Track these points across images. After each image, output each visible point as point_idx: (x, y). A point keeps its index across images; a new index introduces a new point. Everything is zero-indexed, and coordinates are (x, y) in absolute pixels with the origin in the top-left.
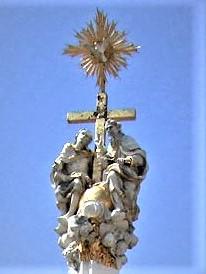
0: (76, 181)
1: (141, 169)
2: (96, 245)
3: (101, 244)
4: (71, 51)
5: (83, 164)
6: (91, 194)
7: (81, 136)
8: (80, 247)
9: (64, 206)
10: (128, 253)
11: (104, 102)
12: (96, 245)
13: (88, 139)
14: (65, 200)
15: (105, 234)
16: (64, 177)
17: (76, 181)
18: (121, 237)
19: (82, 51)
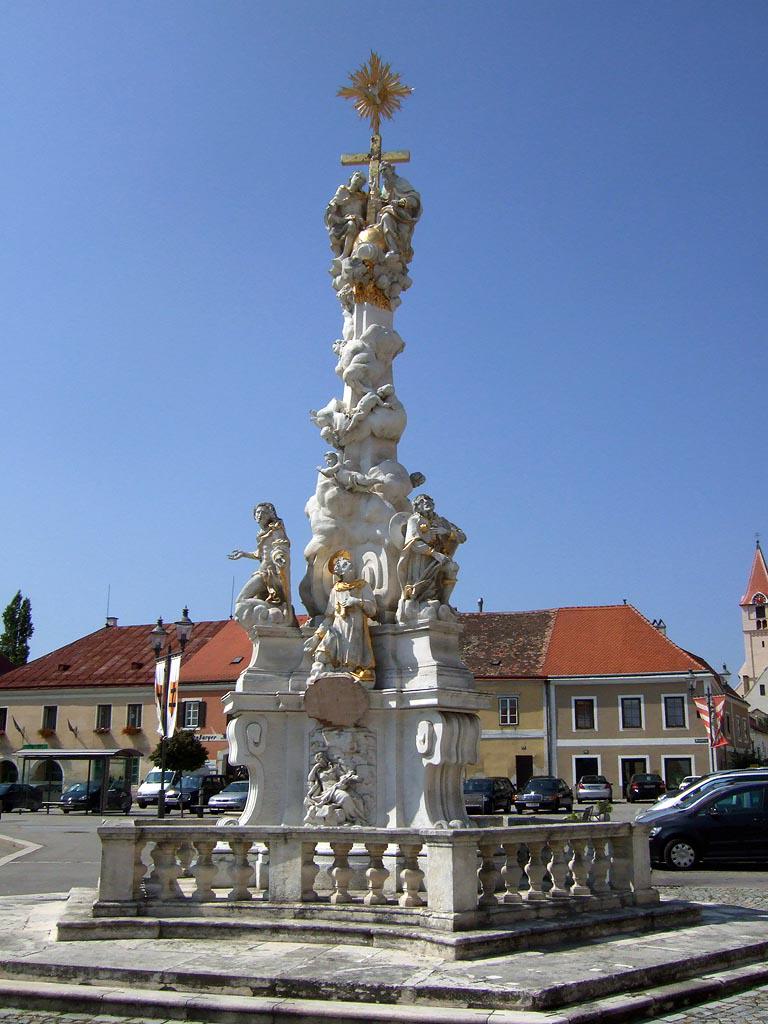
1: (415, 211)
3: (375, 286)
5: (357, 206)
12: (370, 287)
13: (362, 181)
14: (339, 242)
15: (379, 276)
17: (350, 223)
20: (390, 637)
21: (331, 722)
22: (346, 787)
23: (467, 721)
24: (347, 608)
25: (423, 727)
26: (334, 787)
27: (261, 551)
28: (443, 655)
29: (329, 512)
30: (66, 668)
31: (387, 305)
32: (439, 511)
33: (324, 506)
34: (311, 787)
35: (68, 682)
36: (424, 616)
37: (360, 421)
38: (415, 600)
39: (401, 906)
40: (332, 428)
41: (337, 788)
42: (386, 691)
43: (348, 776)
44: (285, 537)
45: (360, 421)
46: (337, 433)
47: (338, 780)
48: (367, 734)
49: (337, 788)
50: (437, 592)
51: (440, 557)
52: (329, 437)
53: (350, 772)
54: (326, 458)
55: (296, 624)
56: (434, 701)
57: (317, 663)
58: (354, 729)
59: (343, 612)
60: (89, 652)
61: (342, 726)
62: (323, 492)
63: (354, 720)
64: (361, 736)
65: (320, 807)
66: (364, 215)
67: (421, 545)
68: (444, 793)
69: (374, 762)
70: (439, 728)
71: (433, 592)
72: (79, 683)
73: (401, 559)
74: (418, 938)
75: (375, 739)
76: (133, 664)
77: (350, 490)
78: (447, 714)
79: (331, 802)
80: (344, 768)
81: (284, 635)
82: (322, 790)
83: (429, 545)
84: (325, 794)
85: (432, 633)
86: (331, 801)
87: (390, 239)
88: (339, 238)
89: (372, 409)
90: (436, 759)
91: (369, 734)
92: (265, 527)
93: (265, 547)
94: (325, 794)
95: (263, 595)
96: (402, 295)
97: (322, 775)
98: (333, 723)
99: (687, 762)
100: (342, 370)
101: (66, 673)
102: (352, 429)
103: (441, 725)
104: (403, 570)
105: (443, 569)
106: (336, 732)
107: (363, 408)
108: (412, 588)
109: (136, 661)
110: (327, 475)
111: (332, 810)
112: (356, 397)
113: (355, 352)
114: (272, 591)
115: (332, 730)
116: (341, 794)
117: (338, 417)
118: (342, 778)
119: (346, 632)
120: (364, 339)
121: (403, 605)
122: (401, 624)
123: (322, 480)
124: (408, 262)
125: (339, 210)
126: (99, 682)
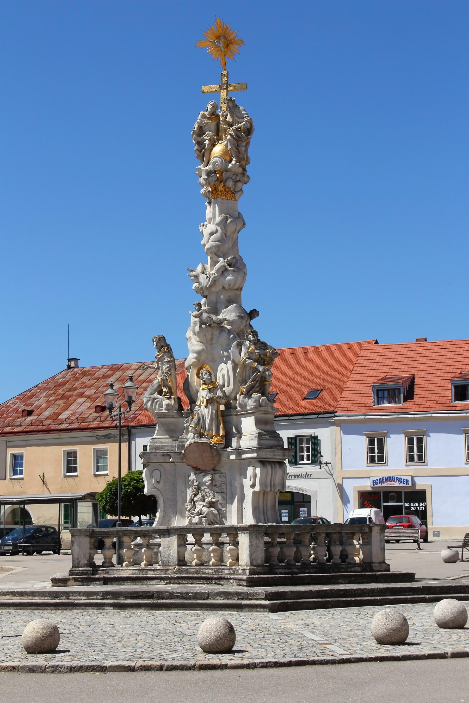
0: (207, 142)
1: (249, 131)
2: (221, 188)
3: (224, 186)
4: (241, 565)
5: (213, 125)
6: (218, 149)
7: (209, 107)
8: (210, 189)
9: (201, 158)
10: (245, 187)
11: (225, 78)
12: (221, 188)
13: (215, 107)
14: (201, 154)
15: (227, 179)
16: (199, 139)
17: (207, 142)
18: (238, 179)
19: (298, 548)
20: (234, 417)
21: (199, 468)
22: (209, 505)
23: (277, 466)
24: (207, 400)
25: (250, 470)
26: (202, 506)
27: (158, 364)
28: (263, 427)
29: (198, 339)
30: (30, 413)
31: (233, 197)
32: (262, 338)
33: (195, 335)
34: (188, 506)
35: (33, 428)
36: (250, 404)
37: (215, 281)
38: (246, 395)
39: (228, 565)
40: (200, 284)
41: (203, 506)
42: (229, 449)
43: (210, 499)
44: (172, 357)
45: (215, 280)
46: (202, 288)
47: (204, 501)
48: (220, 474)
49: (203, 506)
50: (260, 389)
51: (261, 368)
52: (197, 291)
53: (211, 497)
54: (194, 306)
55: (181, 408)
56: (255, 455)
57: (190, 434)
58: (212, 472)
59: (205, 402)
60: (51, 395)
61: (206, 470)
62: (194, 327)
63: (212, 466)
64: (217, 476)
65: (194, 517)
66: (218, 134)
67: (248, 361)
68: (265, 508)
69: (225, 491)
70: (258, 470)
71: (258, 389)
72: (44, 428)
73: (238, 369)
74: (231, 579)
75: (226, 477)
76: (97, 407)
77: (210, 325)
78: (263, 463)
79: (200, 514)
80: (208, 494)
81: (173, 417)
82: (196, 508)
83: (255, 361)
84: (197, 510)
85: (256, 415)
86: (200, 513)
87: (233, 152)
88: (200, 151)
89: (223, 272)
90: (257, 488)
91: (223, 475)
92: (160, 351)
93: (160, 362)
94: (197, 510)
95: (160, 393)
96: (245, 187)
97: (195, 499)
98: (201, 469)
99: (4, 478)
100: (204, 245)
101: (30, 418)
102: (211, 286)
103: (260, 468)
104: (241, 376)
105: (263, 375)
106: (203, 474)
107: (217, 271)
108: (244, 389)
109: (99, 404)
110: (196, 317)
111: (200, 519)
112: (214, 263)
113: (211, 234)
114: (164, 389)
115: (200, 473)
116: (205, 510)
117: (202, 278)
118: (206, 500)
119: (207, 415)
120: (217, 224)
121: (240, 398)
122: (239, 409)
123: (193, 320)
124: (246, 164)
125: (201, 131)
126: (64, 426)
